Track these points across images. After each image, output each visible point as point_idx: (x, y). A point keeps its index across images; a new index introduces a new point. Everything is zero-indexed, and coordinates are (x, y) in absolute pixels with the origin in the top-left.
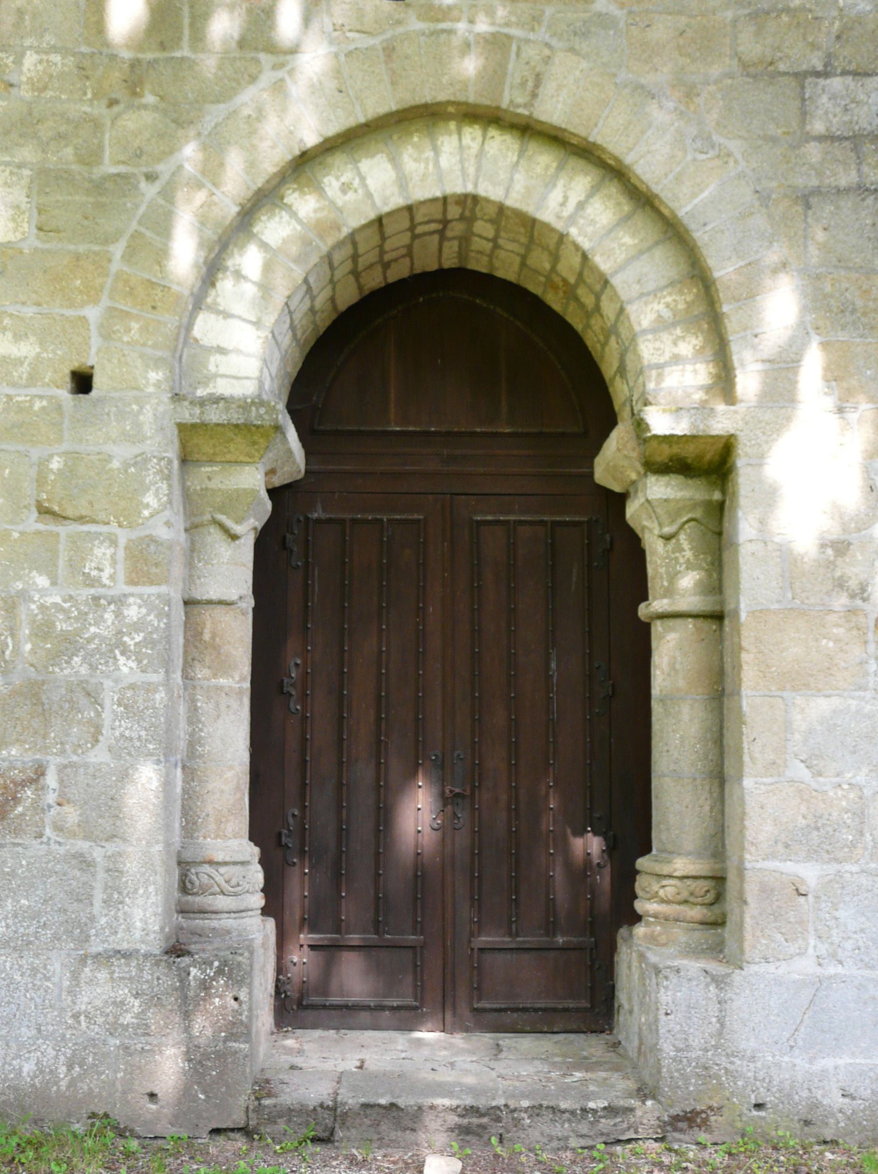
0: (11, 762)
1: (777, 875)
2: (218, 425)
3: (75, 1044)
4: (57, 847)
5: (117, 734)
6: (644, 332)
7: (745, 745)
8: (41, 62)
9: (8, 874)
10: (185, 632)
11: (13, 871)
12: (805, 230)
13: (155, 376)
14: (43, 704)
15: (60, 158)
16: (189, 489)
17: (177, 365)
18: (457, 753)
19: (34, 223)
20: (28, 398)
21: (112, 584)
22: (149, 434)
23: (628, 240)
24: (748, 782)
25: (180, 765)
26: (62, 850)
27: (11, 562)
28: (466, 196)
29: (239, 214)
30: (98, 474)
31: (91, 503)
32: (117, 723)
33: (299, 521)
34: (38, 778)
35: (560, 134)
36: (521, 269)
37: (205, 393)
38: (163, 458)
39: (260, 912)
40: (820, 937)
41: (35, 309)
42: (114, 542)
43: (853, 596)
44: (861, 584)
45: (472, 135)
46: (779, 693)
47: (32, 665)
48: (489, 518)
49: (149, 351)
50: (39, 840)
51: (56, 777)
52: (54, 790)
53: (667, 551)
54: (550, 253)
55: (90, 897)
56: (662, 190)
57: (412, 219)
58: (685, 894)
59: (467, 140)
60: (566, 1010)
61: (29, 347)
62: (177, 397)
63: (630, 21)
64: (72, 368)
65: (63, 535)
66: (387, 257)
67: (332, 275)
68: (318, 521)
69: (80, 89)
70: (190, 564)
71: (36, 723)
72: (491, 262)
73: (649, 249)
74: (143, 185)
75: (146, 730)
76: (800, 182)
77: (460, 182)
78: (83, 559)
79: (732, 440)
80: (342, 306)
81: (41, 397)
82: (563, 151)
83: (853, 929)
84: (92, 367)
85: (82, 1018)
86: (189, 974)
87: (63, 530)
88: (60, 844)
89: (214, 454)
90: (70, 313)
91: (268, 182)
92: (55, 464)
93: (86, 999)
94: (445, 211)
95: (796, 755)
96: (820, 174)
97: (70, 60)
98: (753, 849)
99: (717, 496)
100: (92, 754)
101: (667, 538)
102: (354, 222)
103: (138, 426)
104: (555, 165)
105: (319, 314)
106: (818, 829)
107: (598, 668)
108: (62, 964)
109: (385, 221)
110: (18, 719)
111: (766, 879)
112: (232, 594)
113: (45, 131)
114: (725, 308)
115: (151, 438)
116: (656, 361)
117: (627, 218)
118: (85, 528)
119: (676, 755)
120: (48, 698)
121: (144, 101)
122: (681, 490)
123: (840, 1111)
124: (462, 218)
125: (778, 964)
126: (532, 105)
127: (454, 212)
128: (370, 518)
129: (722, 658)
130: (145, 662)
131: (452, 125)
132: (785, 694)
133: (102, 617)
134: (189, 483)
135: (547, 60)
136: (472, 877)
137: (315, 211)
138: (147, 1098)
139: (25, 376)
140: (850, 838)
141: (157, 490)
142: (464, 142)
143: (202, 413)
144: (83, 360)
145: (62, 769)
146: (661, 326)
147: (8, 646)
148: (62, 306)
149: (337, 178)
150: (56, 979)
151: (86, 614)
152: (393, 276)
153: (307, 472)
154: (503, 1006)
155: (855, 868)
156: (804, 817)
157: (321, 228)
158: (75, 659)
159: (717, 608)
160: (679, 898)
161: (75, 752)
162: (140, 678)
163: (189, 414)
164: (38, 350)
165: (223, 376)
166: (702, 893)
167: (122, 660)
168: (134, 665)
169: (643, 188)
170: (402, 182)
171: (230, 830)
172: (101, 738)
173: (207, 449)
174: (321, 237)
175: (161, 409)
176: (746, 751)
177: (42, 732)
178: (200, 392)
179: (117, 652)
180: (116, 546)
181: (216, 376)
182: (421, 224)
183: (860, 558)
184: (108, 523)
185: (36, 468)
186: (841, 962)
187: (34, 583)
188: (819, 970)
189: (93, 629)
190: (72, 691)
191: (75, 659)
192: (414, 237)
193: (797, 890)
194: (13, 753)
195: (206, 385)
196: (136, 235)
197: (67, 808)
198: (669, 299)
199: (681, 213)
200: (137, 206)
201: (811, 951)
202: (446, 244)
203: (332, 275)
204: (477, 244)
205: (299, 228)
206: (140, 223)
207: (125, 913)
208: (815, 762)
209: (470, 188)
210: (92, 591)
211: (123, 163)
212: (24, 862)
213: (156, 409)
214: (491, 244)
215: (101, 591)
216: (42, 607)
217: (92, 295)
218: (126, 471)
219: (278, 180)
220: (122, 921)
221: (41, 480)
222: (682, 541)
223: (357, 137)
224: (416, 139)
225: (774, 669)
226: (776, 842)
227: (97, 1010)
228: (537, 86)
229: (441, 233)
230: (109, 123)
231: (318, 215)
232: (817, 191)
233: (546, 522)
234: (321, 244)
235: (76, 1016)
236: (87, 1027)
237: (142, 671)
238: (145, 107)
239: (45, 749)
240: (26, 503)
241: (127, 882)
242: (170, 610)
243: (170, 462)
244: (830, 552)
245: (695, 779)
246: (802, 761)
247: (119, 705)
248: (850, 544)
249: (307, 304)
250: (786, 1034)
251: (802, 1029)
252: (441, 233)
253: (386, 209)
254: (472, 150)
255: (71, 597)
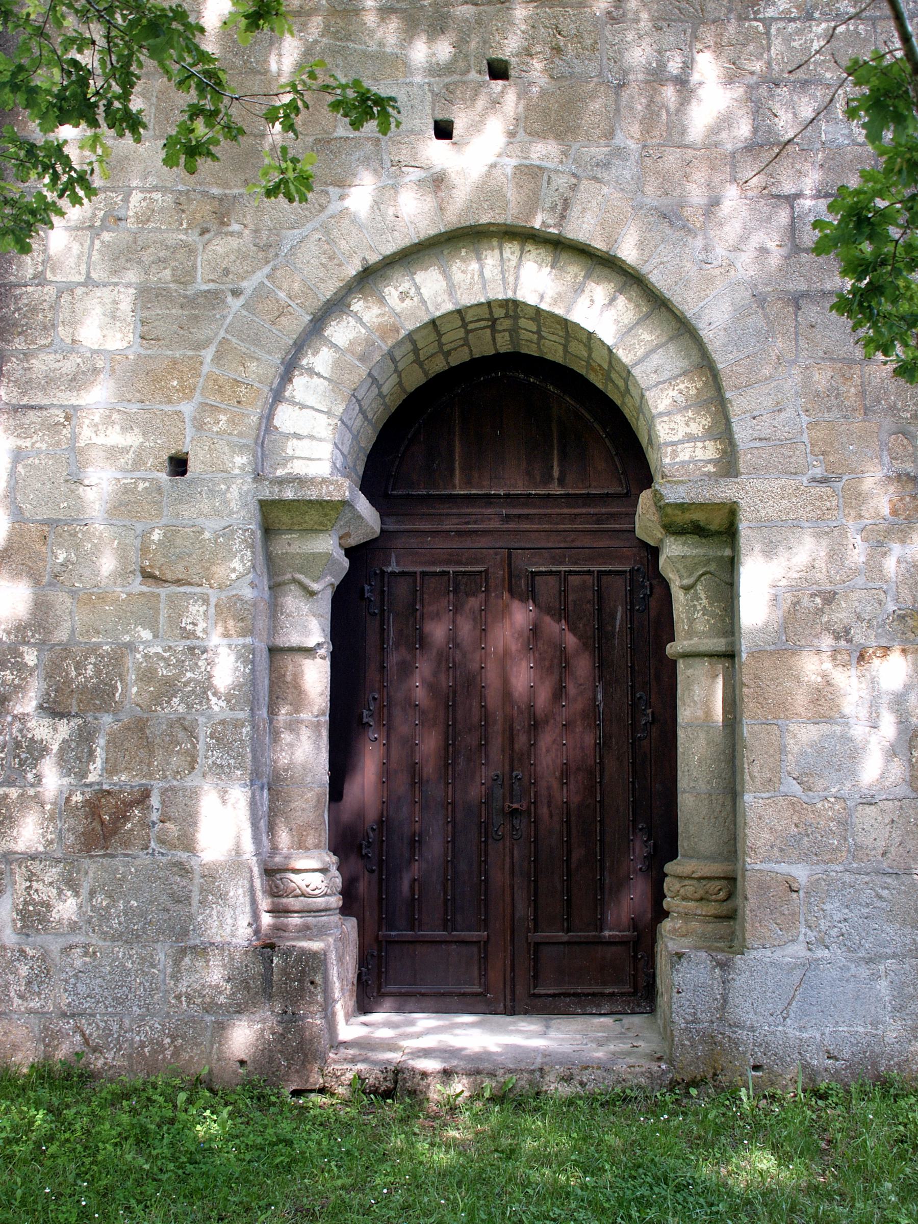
0: (121, 786)
1: (773, 875)
2: (294, 501)
3: (178, 1020)
4: (160, 857)
5: (210, 762)
6: (661, 414)
7: (746, 766)
8: (144, 199)
9: (119, 879)
10: (270, 675)
11: (124, 877)
12: (796, 327)
13: (241, 460)
14: (147, 738)
15: (160, 279)
16: (271, 552)
17: (259, 450)
18: (515, 773)
19: (138, 333)
20: (133, 481)
21: (205, 636)
22: (235, 509)
23: (646, 336)
24: (748, 798)
25: (266, 787)
26: (164, 860)
27: (120, 619)
28: (507, 301)
29: (311, 321)
30: (192, 543)
31: (186, 568)
32: (210, 753)
33: (376, 574)
34: (144, 799)
35: (585, 248)
36: (565, 355)
37: (283, 473)
38: (248, 530)
39: (338, 911)
40: (810, 927)
41: (139, 405)
42: (206, 601)
43: (837, 638)
44: (845, 627)
45: (511, 250)
46: (775, 721)
47: (138, 705)
48: (542, 569)
49: (236, 439)
50: (145, 852)
51: (159, 798)
52: (158, 810)
53: (687, 600)
54: (585, 345)
55: (188, 898)
56: (673, 295)
57: (463, 319)
58: (701, 893)
59: (507, 253)
60: (613, 994)
61: (134, 438)
62: (258, 477)
63: (644, 154)
64: (169, 454)
65: (163, 596)
66: (446, 348)
67: (396, 367)
68: (393, 574)
69: (177, 220)
70: (274, 617)
71: (143, 753)
72: (539, 347)
73: (667, 342)
74: (230, 299)
75: (234, 758)
76: (791, 287)
77: (501, 289)
78: (180, 616)
79: (735, 506)
80: (411, 388)
81: (144, 480)
82: (590, 262)
83: (838, 919)
84: (187, 453)
85: (183, 999)
86: (272, 962)
87: (163, 591)
88: (163, 854)
89: (292, 524)
90: (168, 408)
91: (335, 294)
92: (156, 536)
93: (186, 984)
94: (491, 313)
95: (789, 774)
96: (809, 280)
97: (169, 198)
98: (752, 854)
99: (728, 552)
100: (188, 779)
101: (687, 589)
102: (410, 326)
103: (226, 502)
104: (583, 274)
105: (387, 398)
106: (808, 836)
107: (640, 698)
108: (166, 954)
109: (438, 323)
110: (127, 750)
111: (763, 878)
112: (311, 643)
113: (147, 257)
114: (728, 395)
115: (237, 512)
116: (670, 439)
117: (647, 316)
118: (182, 589)
119: (695, 774)
120: (151, 733)
121: (230, 229)
122: (696, 548)
123: (826, 1071)
124: (507, 316)
125: (773, 949)
126: (561, 225)
127: (499, 312)
128: (438, 570)
129: (734, 691)
130: (233, 701)
131: (495, 243)
132: (780, 722)
133: (197, 664)
134: (271, 549)
135: (574, 188)
136: (529, 881)
137: (377, 316)
138: (238, 1064)
139: (130, 462)
140: (836, 842)
141: (242, 556)
142: (505, 256)
143: (280, 491)
144: (179, 448)
145: (164, 792)
146: (676, 408)
147: (117, 687)
148: (161, 402)
149: (396, 288)
150: (161, 967)
151: (183, 661)
152: (455, 361)
153: (382, 531)
154: (556, 992)
155: (840, 868)
156: (796, 826)
157: (386, 330)
158: (174, 699)
159: (729, 648)
160: (697, 896)
161: (175, 778)
162: (228, 715)
163: (268, 492)
164: (141, 440)
165: (297, 458)
166: (715, 891)
167: (214, 700)
168: (224, 704)
169: (658, 293)
170: (451, 289)
171: (311, 842)
172: (197, 766)
173: (285, 519)
174: (383, 339)
175: (245, 488)
176: (746, 771)
177: (147, 761)
178: (280, 472)
179: (209, 693)
180: (208, 604)
181: (293, 458)
182: (471, 322)
183: (844, 606)
184: (201, 585)
185: (139, 539)
186: (827, 947)
187: (139, 636)
188: (809, 954)
189: (189, 675)
190: (171, 727)
191: (174, 699)
192: (468, 332)
193: (790, 887)
194: (123, 779)
195: (285, 465)
196: (224, 341)
197: (168, 825)
198: (682, 386)
199: (689, 314)
200: (224, 317)
201: (801, 938)
202: (498, 336)
203: (396, 367)
204: (524, 335)
205: (363, 331)
206: (227, 332)
207: (218, 912)
208: (805, 779)
209: (510, 295)
210: (188, 642)
211: (213, 281)
212: (133, 870)
213: (240, 488)
214: (536, 336)
215: (196, 642)
216: (145, 655)
217: (187, 392)
218: (216, 541)
219: (344, 292)
220: (215, 918)
221: (144, 550)
222: (699, 591)
223: (412, 253)
224: (463, 254)
225: (770, 701)
226: (772, 847)
227: (195, 992)
228: (565, 209)
229: (493, 327)
230: (201, 248)
231: (380, 320)
232: (805, 295)
233: (593, 572)
234: (383, 345)
235: (178, 997)
236: (188, 1006)
237: (231, 709)
238: (232, 234)
239: (150, 775)
240: (132, 569)
241: (219, 886)
242: (254, 657)
243: (253, 532)
244: (818, 600)
245: (710, 795)
246: (794, 778)
247: (212, 738)
248: (835, 593)
249: (375, 391)
250: (780, 1007)
251: (794, 1004)
252: (493, 327)
253: (438, 314)
254: (511, 262)
255: (170, 647)
